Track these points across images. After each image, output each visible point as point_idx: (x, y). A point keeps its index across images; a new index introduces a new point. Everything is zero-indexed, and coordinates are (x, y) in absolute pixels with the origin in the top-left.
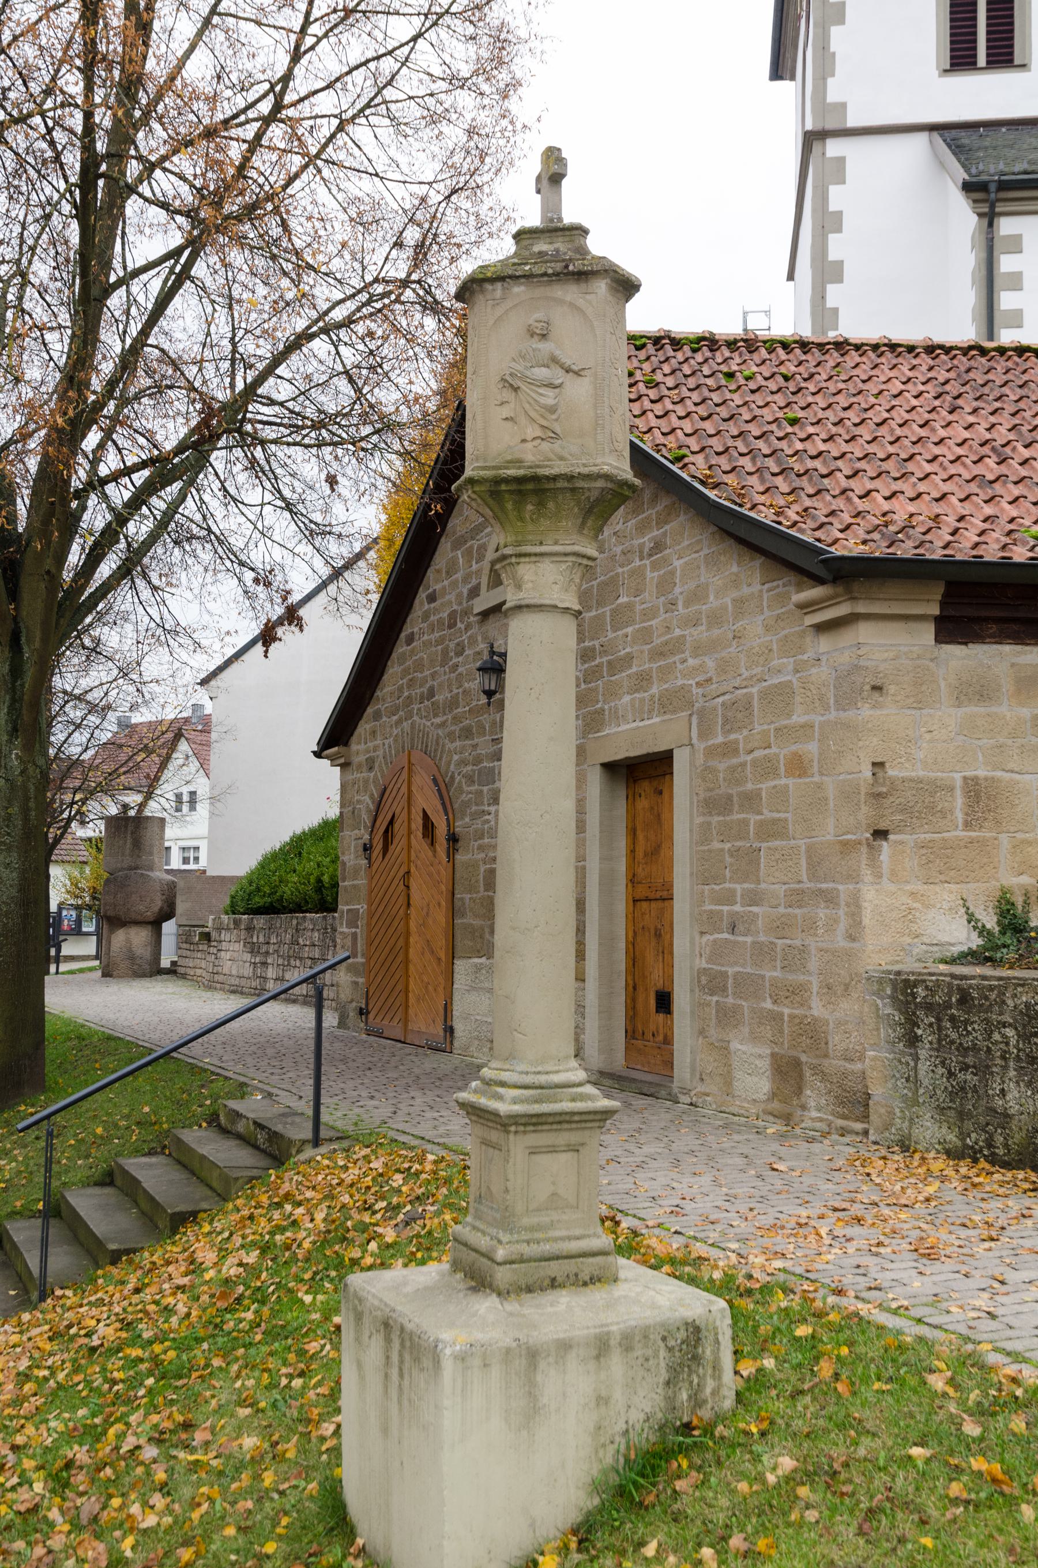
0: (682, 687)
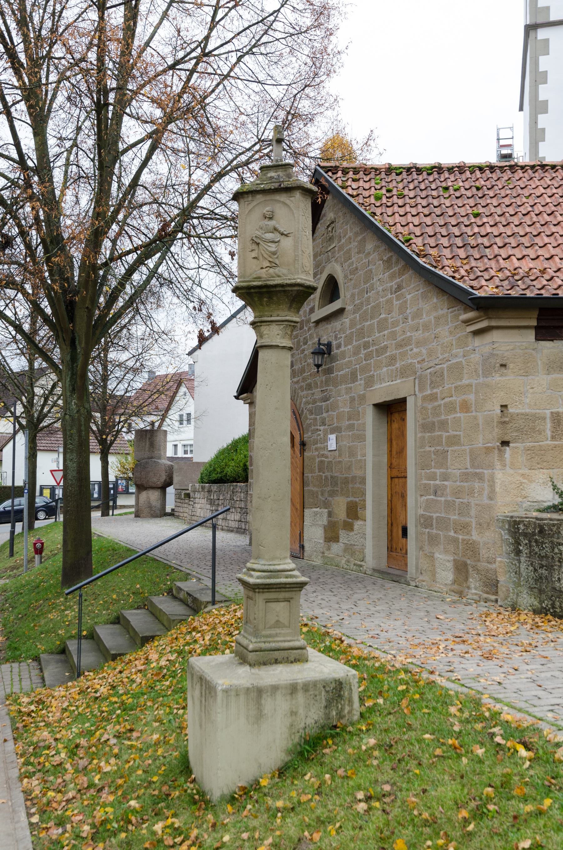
0: (411, 364)
